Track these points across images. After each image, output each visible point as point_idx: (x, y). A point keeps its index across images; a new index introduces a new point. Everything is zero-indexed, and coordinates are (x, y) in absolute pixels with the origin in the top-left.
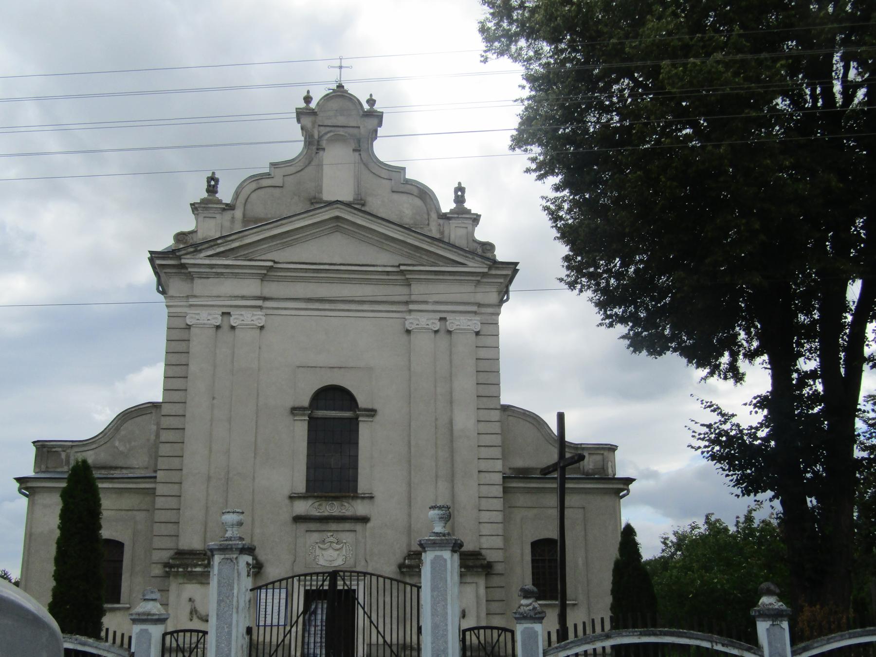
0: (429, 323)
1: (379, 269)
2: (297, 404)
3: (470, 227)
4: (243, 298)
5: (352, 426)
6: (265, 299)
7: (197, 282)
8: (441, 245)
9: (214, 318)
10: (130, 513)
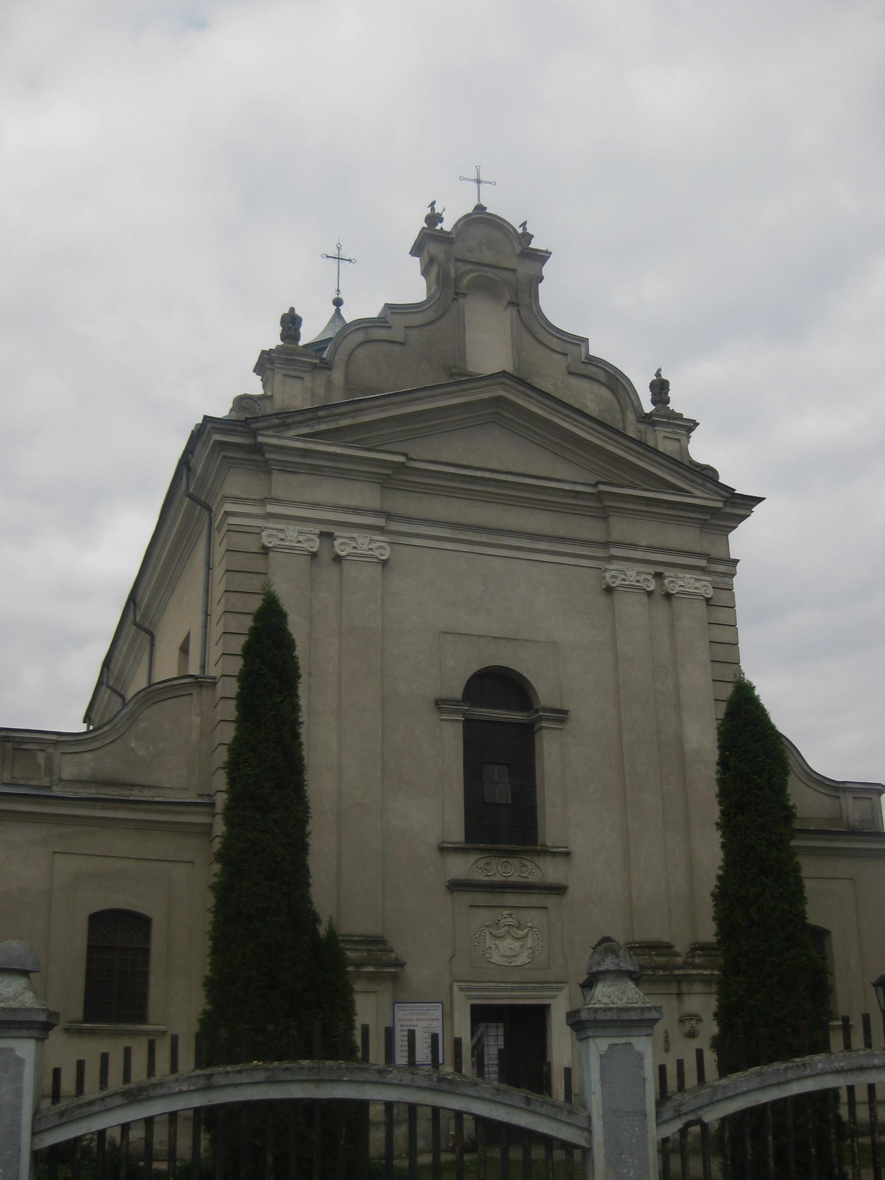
0: (641, 578)
1: (567, 487)
4: (355, 510)
5: (526, 734)
6: (389, 516)
7: (276, 476)
8: (657, 458)
9: (308, 540)
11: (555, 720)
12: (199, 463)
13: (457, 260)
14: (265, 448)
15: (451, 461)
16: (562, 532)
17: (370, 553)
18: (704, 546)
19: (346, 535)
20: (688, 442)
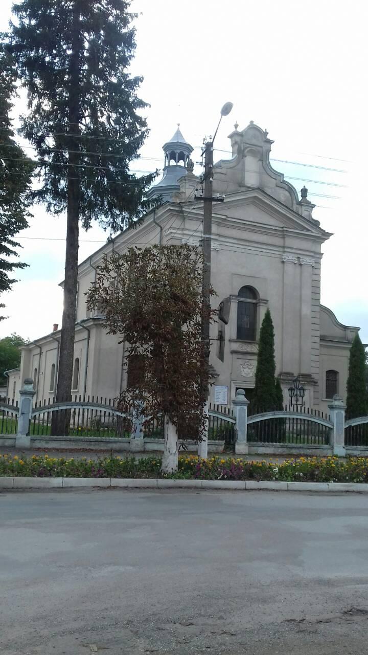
9: (196, 243)
18: (313, 249)
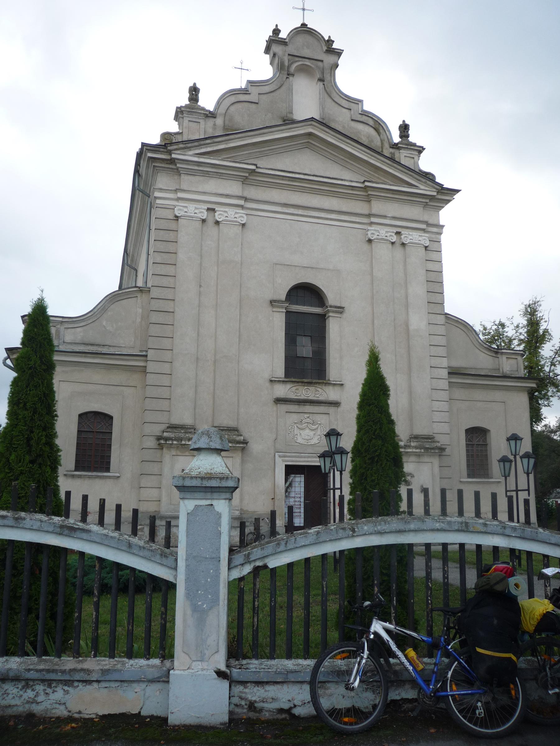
2: (275, 298)
3: (416, 158)
4: (227, 196)
5: (322, 318)
6: (246, 199)
8: (399, 167)
9: (201, 212)
10: (118, 388)
11: (336, 312)
12: (143, 171)
13: (289, 55)
14: (176, 161)
15: (283, 169)
16: (344, 209)
17: (235, 219)
18: (426, 218)
19: (222, 209)
20: (419, 160)
